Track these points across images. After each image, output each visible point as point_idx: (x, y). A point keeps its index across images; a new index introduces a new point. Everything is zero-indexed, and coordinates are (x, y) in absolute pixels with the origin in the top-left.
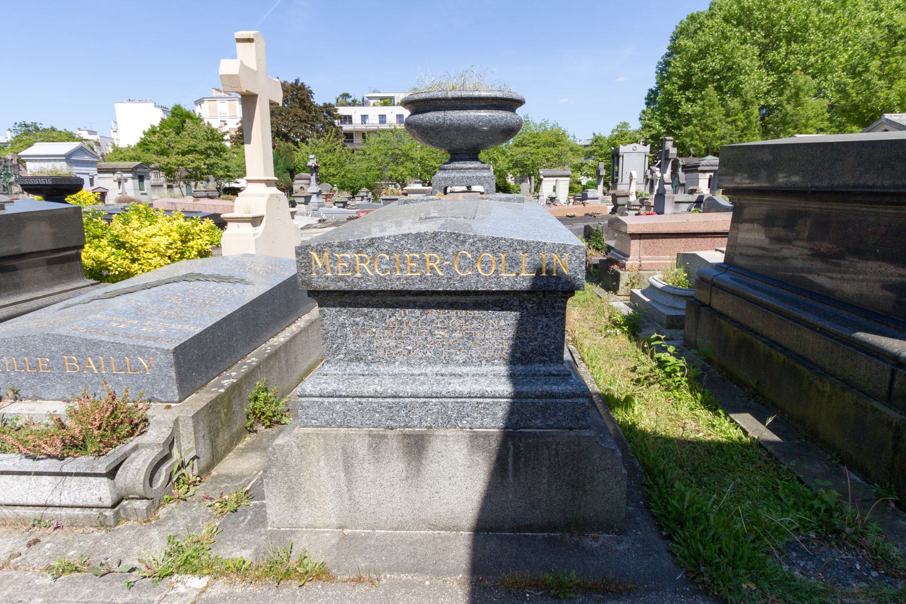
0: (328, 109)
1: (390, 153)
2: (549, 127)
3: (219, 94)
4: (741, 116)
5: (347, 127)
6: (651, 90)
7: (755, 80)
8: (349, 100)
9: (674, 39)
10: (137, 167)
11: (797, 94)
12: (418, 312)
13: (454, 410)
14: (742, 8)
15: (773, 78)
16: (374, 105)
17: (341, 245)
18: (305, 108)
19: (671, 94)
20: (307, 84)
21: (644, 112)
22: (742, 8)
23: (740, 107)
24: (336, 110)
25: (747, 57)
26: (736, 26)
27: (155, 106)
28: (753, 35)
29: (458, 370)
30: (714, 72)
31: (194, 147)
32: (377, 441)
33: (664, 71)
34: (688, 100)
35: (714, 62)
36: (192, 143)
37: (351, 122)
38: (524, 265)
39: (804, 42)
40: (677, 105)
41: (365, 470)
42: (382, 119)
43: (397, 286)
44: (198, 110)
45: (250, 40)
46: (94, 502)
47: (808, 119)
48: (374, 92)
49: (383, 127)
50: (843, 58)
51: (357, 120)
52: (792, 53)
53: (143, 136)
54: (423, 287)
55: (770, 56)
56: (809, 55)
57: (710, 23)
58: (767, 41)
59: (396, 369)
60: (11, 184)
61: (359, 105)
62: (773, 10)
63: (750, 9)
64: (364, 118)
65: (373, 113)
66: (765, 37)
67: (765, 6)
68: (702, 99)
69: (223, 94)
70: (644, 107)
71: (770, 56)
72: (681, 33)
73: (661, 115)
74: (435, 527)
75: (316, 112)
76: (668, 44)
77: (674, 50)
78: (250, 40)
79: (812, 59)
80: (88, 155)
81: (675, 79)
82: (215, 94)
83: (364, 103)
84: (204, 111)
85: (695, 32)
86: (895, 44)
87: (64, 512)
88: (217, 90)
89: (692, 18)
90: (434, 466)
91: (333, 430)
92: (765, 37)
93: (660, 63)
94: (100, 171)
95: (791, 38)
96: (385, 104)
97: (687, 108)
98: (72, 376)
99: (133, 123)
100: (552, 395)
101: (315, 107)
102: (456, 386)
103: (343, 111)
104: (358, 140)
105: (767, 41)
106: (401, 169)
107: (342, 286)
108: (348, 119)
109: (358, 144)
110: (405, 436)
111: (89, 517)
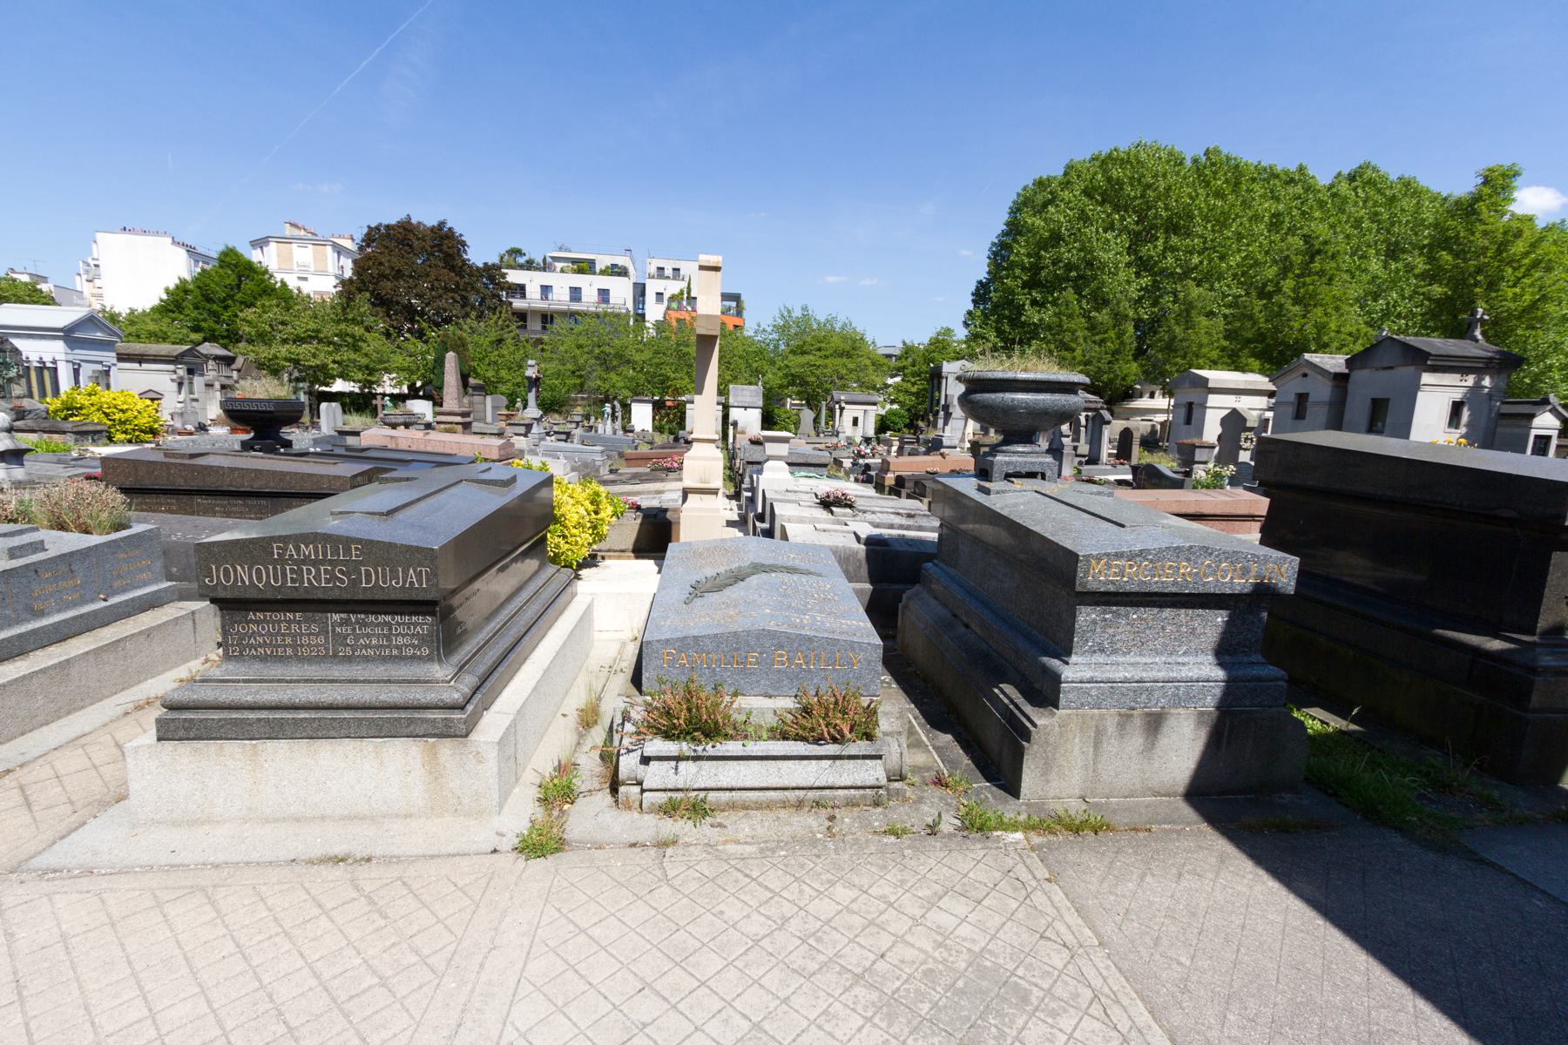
0: (492, 273)
1: (597, 351)
2: (838, 326)
3: (296, 232)
4: (1112, 334)
5: (518, 304)
6: (980, 282)
7: (1124, 283)
8: (521, 260)
9: (1016, 210)
10: (183, 355)
11: (1188, 311)
12: (1156, 610)
13: (1183, 691)
14: (1109, 180)
15: (1145, 281)
16: (562, 271)
17: (1116, 555)
18: (452, 268)
19: (1013, 293)
20: (458, 230)
21: (970, 313)
22: (1109, 180)
23: (1111, 323)
24: (504, 276)
25: (1112, 250)
26: (1102, 204)
27: (174, 242)
28: (1123, 219)
29: (1180, 660)
30: (1069, 267)
31: (318, 331)
32: (1125, 719)
33: (1000, 255)
34: (1034, 303)
35: (1068, 254)
36: (312, 325)
37: (523, 296)
38: (1253, 573)
39: (1188, 235)
40: (1020, 309)
41: (1111, 746)
42: (576, 293)
43: (1154, 589)
44: (255, 256)
45: (717, 269)
46: (871, 781)
47: (1201, 346)
48: (560, 249)
49: (575, 307)
50: (1235, 260)
51: (533, 292)
52: (1174, 249)
53: (165, 297)
54: (1174, 590)
55: (1146, 250)
56: (1191, 253)
57: (1066, 195)
58: (1139, 228)
59: (1130, 658)
60: (10, 380)
61: (537, 269)
62: (1149, 186)
63: (1120, 183)
64: (546, 290)
65: (561, 284)
66: (1137, 223)
67: (1139, 180)
68: (1055, 303)
69: (302, 233)
70: (971, 307)
71: (1146, 250)
72: (1025, 203)
73: (997, 321)
74: (1157, 794)
75: (471, 275)
76: (1005, 217)
77: (1014, 229)
78: (717, 269)
79: (1196, 260)
80: (102, 330)
81: (1018, 272)
82: (289, 231)
83: (545, 267)
84: (269, 259)
85: (1045, 205)
86: (1312, 261)
87: (840, 792)
88: (293, 225)
89: (1041, 184)
90: (1166, 740)
91: (1087, 710)
92: (1137, 223)
93: (994, 244)
94: (123, 358)
95: (1172, 227)
96: (581, 271)
97: (1032, 315)
98: (779, 671)
99: (139, 272)
100: (1259, 679)
101: (470, 267)
102: (1185, 673)
103: (514, 276)
104: (535, 325)
105: (1139, 228)
106: (613, 376)
107: (1112, 588)
108: (520, 290)
109: (535, 332)
110: (1148, 715)
111: (863, 797)
